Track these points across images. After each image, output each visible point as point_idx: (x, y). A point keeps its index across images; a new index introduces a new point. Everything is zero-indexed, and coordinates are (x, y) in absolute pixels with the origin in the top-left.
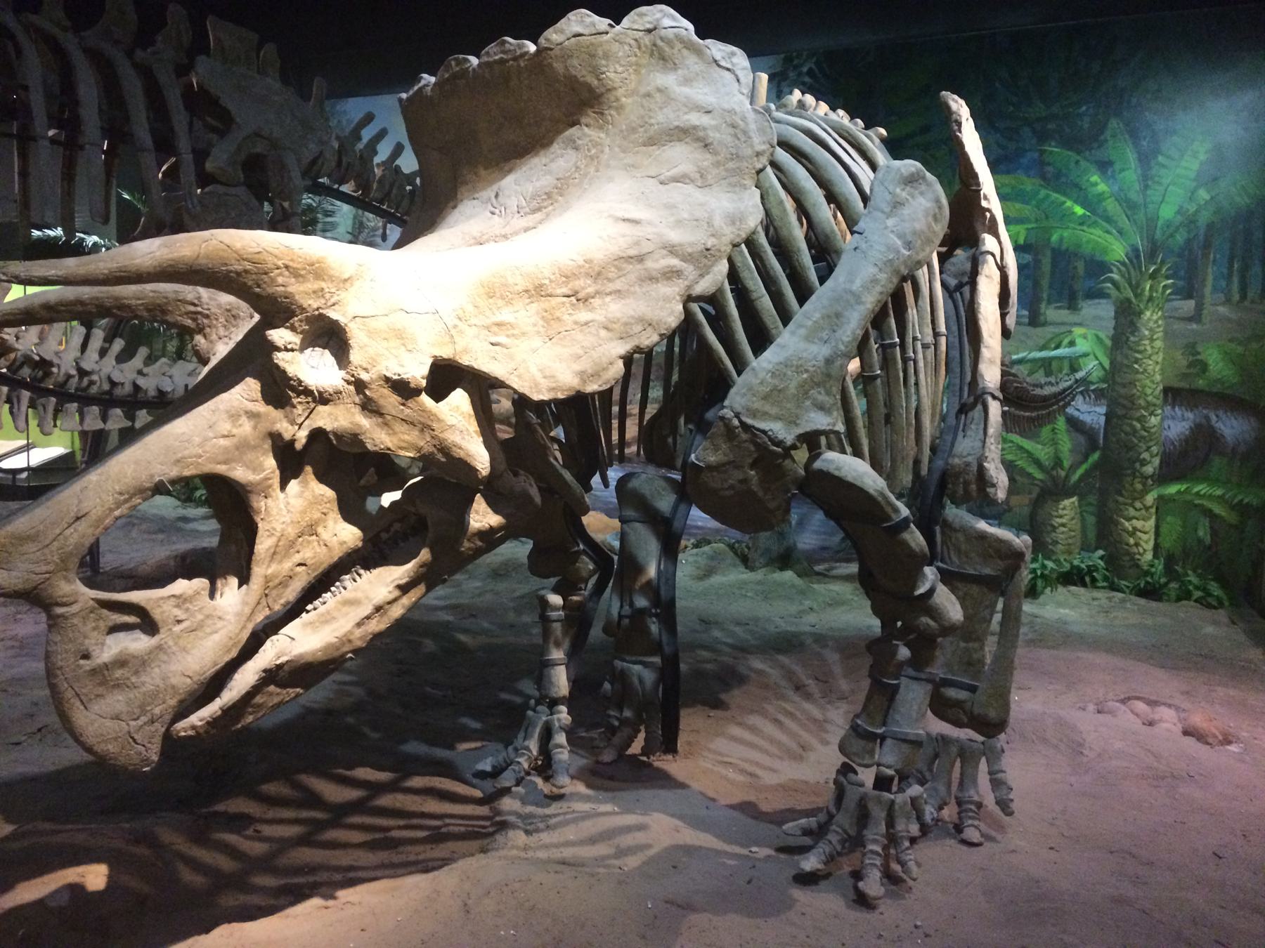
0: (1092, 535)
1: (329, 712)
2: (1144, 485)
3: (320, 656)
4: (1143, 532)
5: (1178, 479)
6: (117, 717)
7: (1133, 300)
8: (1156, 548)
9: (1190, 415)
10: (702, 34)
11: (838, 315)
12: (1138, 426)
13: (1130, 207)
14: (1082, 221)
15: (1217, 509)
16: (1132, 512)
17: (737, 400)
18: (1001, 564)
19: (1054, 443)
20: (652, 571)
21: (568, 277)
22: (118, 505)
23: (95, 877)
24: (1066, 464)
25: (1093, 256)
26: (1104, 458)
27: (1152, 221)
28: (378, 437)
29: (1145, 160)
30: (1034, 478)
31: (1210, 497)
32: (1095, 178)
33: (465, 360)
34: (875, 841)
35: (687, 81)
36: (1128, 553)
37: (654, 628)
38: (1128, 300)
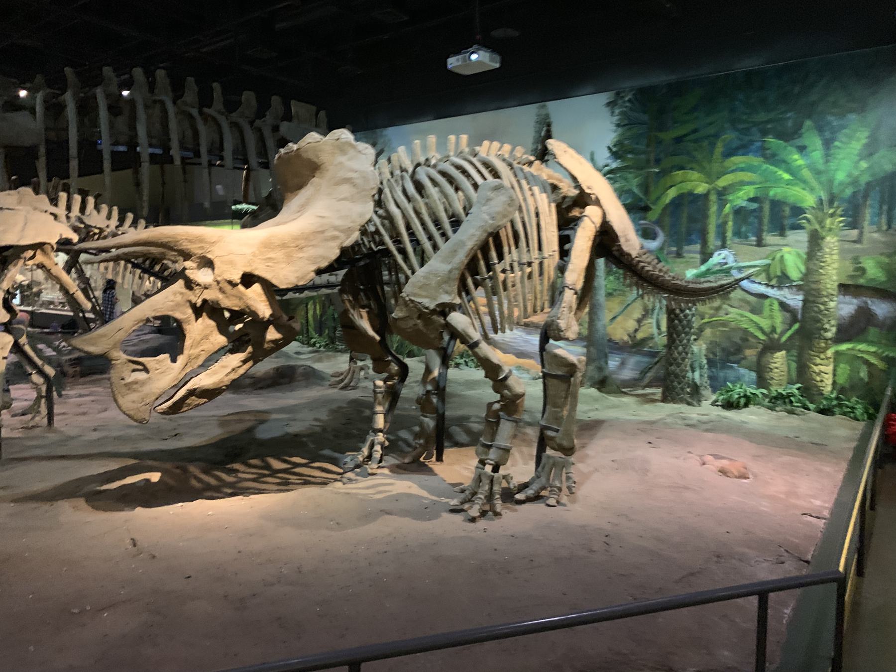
0: (794, 374)
1: (296, 435)
2: (826, 343)
3: (212, 387)
4: (826, 373)
5: (848, 340)
6: (134, 402)
7: (819, 230)
8: (834, 383)
9: (855, 301)
10: (357, 140)
11: (455, 251)
12: (822, 307)
13: (817, 173)
14: (788, 183)
15: (873, 360)
16: (818, 361)
17: (407, 290)
18: (566, 369)
19: (771, 317)
20: (436, 373)
21: (296, 239)
22: (134, 325)
23: (155, 477)
24: (779, 330)
25: (485, 231)
26: (801, 328)
27: (831, 182)
28: (225, 302)
29: (828, 144)
30: (759, 339)
31: (868, 352)
32: (796, 157)
33: (257, 273)
34: (482, 493)
35: (349, 160)
36: (817, 387)
37: (435, 400)
38: (816, 230)
